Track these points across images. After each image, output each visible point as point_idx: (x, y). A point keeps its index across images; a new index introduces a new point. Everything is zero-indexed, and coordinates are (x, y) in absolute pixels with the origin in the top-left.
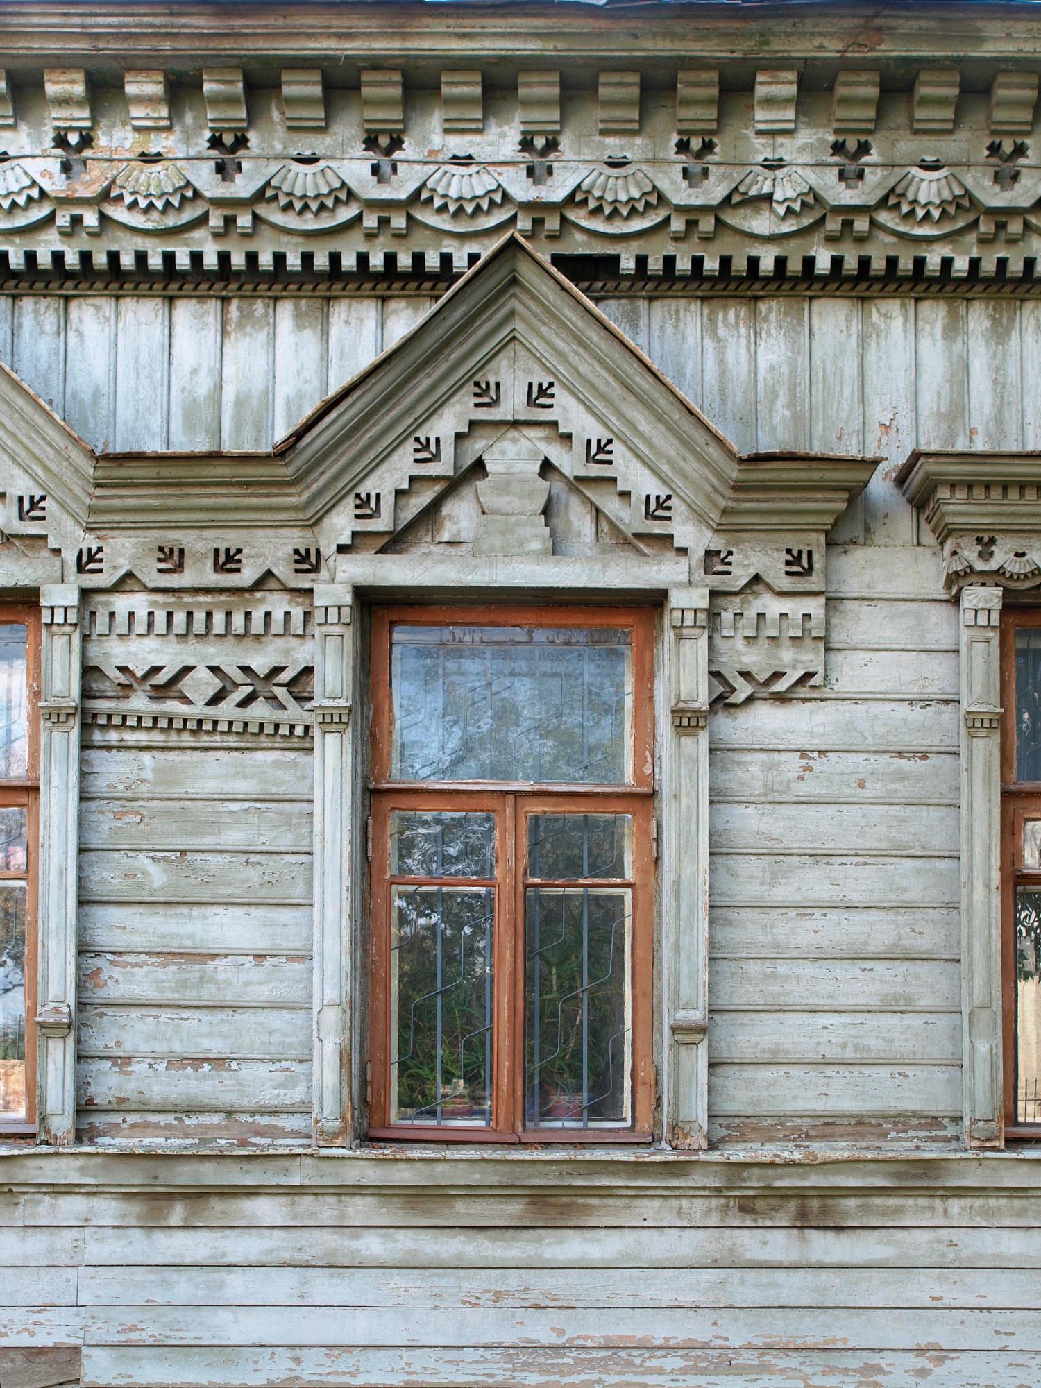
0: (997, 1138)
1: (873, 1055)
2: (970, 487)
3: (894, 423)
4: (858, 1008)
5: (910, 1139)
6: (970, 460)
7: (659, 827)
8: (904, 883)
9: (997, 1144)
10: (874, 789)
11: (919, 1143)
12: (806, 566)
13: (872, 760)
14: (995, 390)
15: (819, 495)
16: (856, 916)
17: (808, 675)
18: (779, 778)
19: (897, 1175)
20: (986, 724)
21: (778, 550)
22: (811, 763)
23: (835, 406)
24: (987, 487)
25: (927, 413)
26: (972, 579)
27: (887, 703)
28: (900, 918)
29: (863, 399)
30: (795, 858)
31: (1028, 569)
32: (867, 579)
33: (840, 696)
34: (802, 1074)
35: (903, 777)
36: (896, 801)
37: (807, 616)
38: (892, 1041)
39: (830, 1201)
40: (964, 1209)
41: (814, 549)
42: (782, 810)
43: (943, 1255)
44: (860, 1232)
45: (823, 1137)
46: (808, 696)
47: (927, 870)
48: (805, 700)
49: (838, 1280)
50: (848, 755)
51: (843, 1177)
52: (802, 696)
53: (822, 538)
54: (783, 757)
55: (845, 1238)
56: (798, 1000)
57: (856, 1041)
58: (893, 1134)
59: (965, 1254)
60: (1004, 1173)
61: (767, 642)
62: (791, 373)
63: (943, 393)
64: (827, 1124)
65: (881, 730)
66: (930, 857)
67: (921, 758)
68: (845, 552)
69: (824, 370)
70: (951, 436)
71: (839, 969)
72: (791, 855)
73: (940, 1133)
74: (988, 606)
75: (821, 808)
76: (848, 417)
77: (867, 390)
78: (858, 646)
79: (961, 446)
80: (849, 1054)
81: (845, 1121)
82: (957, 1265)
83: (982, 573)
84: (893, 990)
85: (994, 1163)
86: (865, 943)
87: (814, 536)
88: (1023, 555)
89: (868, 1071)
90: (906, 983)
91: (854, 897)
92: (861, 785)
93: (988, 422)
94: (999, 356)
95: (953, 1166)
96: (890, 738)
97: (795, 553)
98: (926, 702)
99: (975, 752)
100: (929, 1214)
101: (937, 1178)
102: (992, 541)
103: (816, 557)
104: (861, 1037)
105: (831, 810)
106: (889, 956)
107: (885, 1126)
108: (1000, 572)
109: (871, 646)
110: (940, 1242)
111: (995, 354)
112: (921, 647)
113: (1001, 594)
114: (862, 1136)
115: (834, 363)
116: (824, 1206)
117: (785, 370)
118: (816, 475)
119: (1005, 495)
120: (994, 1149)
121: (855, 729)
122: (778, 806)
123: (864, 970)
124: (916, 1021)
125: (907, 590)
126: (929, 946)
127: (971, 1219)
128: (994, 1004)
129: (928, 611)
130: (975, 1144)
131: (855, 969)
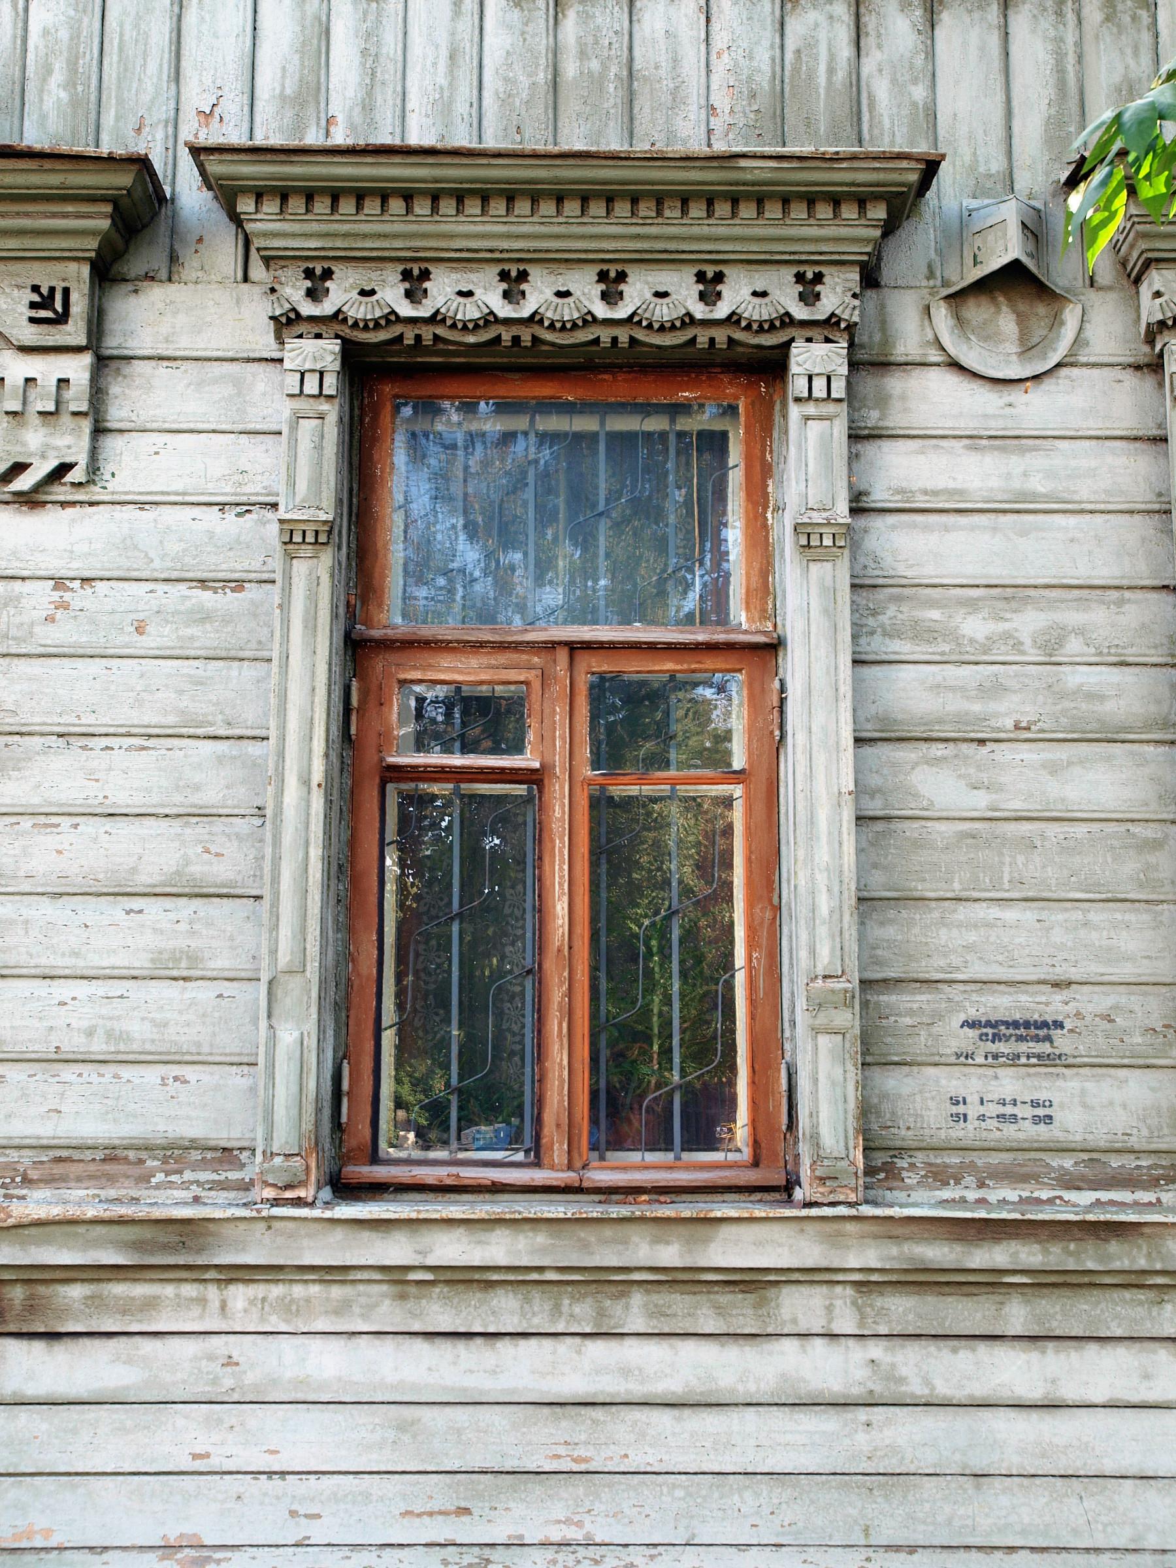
0: (303, 1184)
1: (135, 1047)
2: (284, 197)
3: (217, 110)
4: (116, 972)
5: (186, 1185)
6: (269, 157)
7: (783, 690)
8: (198, 777)
9: (302, 1193)
10: (158, 637)
11: (195, 1190)
12: (59, 309)
13: (160, 593)
14: (363, 65)
15: (70, 208)
16: (121, 827)
17: (64, 469)
18: (18, 620)
19: (138, 1246)
20: (310, 538)
21: (19, 287)
22: (67, 596)
23: (135, 85)
24: (310, 196)
25: (266, 96)
26: (302, 328)
27: (187, 508)
28: (188, 831)
29: (177, 76)
30: (36, 739)
31: (378, 314)
32: (164, 329)
33: (117, 498)
34: (23, 1077)
35: (204, 617)
36: (192, 653)
37: (63, 382)
38: (166, 1025)
39: (42, 1290)
40: (252, 1302)
41: (73, 286)
42: (22, 666)
43: (215, 1381)
44: (86, 1341)
45: (49, 1181)
46: (70, 498)
47: (234, 758)
48: (64, 504)
49: (44, 1426)
50: (125, 584)
51: (52, 1249)
52: (62, 498)
53: (86, 270)
54: (29, 586)
55: (62, 1352)
56: (24, 959)
57: (109, 1024)
58: (160, 1177)
59: (250, 1378)
60: (305, 1242)
61: (6, 418)
62: (71, 39)
63: (291, 69)
64: (59, 1160)
65: (174, 547)
66: (241, 738)
67: (233, 590)
68: (136, 291)
69: (121, 35)
70: (299, 126)
71: (90, 910)
72: (30, 734)
73: (234, 1175)
74: (318, 367)
75: (79, 663)
76: (152, 101)
77: (183, 64)
78: (149, 426)
79: (312, 138)
80: (98, 1046)
81: (88, 1155)
82: (236, 1398)
83: (312, 319)
84: (171, 944)
85: (291, 1225)
86: (134, 870)
87: (73, 266)
88: (372, 292)
89: (126, 1072)
90: (192, 933)
91: (121, 799)
92: (140, 630)
93: (351, 109)
94: (371, 17)
95: (228, 1230)
96: (187, 559)
97: (45, 291)
98: (245, 507)
99: (295, 580)
100: (196, 1311)
101: (200, 1250)
102: (328, 274)
103: (74, 297)
104: (119, 1018)
105: (96, 666)
106: (168, 890)
107: (149, 1163)
108: (337, 317)
109: (167, 426)
110: (211, 1358)
111: (365, 13)
112: (241, 427)
113: (337, 349)
114: (111, 1179)
115: (136, 26)
116: (31, 1297)
117: (64, 34)
118: (54, 179)
119: (334, 208)
120: (298, 1202)
121: (136, 547)
122: (16, 660)
123: (128, 913)
124: (203, 993)
125: (223, 345)
126: (231, 875)
127: (262, 1319)
128: (309, 968)
129: (254, 375)
130: (269, 1193)
131: (115, 910)
